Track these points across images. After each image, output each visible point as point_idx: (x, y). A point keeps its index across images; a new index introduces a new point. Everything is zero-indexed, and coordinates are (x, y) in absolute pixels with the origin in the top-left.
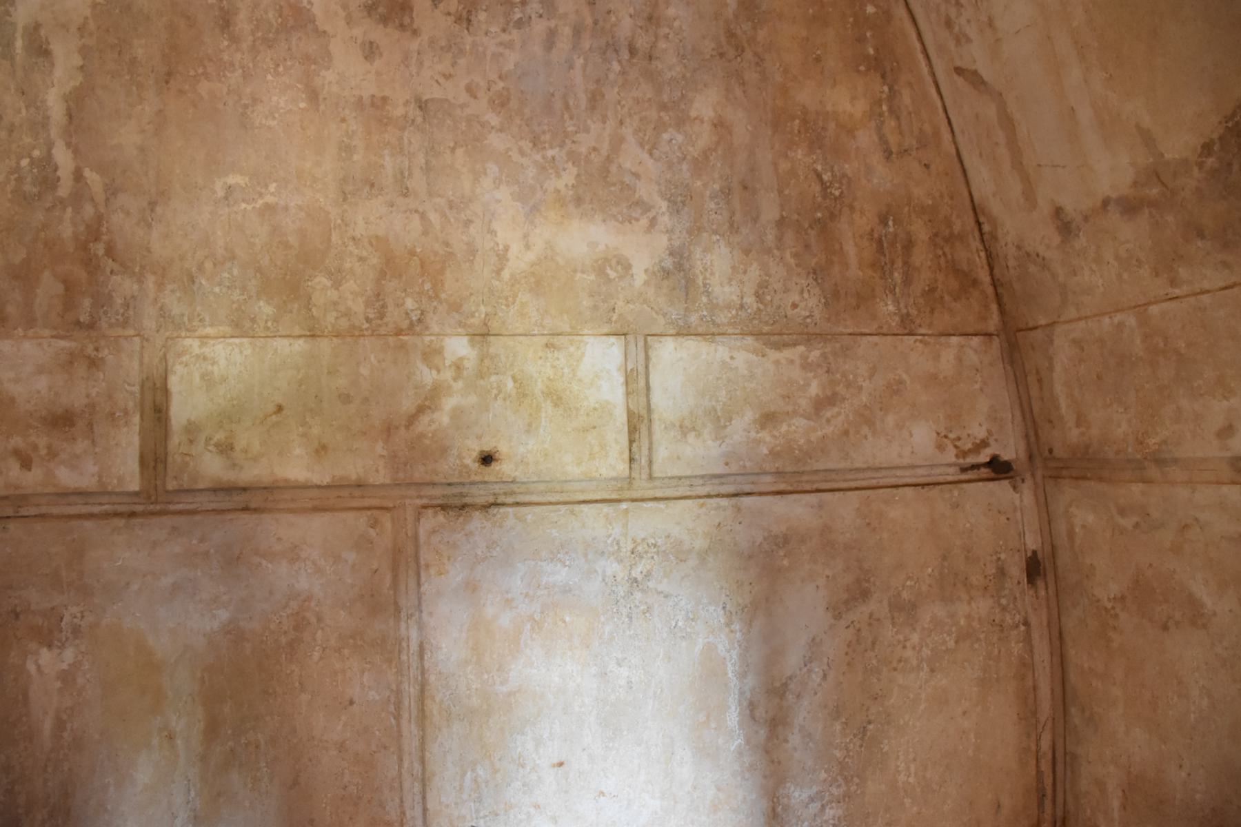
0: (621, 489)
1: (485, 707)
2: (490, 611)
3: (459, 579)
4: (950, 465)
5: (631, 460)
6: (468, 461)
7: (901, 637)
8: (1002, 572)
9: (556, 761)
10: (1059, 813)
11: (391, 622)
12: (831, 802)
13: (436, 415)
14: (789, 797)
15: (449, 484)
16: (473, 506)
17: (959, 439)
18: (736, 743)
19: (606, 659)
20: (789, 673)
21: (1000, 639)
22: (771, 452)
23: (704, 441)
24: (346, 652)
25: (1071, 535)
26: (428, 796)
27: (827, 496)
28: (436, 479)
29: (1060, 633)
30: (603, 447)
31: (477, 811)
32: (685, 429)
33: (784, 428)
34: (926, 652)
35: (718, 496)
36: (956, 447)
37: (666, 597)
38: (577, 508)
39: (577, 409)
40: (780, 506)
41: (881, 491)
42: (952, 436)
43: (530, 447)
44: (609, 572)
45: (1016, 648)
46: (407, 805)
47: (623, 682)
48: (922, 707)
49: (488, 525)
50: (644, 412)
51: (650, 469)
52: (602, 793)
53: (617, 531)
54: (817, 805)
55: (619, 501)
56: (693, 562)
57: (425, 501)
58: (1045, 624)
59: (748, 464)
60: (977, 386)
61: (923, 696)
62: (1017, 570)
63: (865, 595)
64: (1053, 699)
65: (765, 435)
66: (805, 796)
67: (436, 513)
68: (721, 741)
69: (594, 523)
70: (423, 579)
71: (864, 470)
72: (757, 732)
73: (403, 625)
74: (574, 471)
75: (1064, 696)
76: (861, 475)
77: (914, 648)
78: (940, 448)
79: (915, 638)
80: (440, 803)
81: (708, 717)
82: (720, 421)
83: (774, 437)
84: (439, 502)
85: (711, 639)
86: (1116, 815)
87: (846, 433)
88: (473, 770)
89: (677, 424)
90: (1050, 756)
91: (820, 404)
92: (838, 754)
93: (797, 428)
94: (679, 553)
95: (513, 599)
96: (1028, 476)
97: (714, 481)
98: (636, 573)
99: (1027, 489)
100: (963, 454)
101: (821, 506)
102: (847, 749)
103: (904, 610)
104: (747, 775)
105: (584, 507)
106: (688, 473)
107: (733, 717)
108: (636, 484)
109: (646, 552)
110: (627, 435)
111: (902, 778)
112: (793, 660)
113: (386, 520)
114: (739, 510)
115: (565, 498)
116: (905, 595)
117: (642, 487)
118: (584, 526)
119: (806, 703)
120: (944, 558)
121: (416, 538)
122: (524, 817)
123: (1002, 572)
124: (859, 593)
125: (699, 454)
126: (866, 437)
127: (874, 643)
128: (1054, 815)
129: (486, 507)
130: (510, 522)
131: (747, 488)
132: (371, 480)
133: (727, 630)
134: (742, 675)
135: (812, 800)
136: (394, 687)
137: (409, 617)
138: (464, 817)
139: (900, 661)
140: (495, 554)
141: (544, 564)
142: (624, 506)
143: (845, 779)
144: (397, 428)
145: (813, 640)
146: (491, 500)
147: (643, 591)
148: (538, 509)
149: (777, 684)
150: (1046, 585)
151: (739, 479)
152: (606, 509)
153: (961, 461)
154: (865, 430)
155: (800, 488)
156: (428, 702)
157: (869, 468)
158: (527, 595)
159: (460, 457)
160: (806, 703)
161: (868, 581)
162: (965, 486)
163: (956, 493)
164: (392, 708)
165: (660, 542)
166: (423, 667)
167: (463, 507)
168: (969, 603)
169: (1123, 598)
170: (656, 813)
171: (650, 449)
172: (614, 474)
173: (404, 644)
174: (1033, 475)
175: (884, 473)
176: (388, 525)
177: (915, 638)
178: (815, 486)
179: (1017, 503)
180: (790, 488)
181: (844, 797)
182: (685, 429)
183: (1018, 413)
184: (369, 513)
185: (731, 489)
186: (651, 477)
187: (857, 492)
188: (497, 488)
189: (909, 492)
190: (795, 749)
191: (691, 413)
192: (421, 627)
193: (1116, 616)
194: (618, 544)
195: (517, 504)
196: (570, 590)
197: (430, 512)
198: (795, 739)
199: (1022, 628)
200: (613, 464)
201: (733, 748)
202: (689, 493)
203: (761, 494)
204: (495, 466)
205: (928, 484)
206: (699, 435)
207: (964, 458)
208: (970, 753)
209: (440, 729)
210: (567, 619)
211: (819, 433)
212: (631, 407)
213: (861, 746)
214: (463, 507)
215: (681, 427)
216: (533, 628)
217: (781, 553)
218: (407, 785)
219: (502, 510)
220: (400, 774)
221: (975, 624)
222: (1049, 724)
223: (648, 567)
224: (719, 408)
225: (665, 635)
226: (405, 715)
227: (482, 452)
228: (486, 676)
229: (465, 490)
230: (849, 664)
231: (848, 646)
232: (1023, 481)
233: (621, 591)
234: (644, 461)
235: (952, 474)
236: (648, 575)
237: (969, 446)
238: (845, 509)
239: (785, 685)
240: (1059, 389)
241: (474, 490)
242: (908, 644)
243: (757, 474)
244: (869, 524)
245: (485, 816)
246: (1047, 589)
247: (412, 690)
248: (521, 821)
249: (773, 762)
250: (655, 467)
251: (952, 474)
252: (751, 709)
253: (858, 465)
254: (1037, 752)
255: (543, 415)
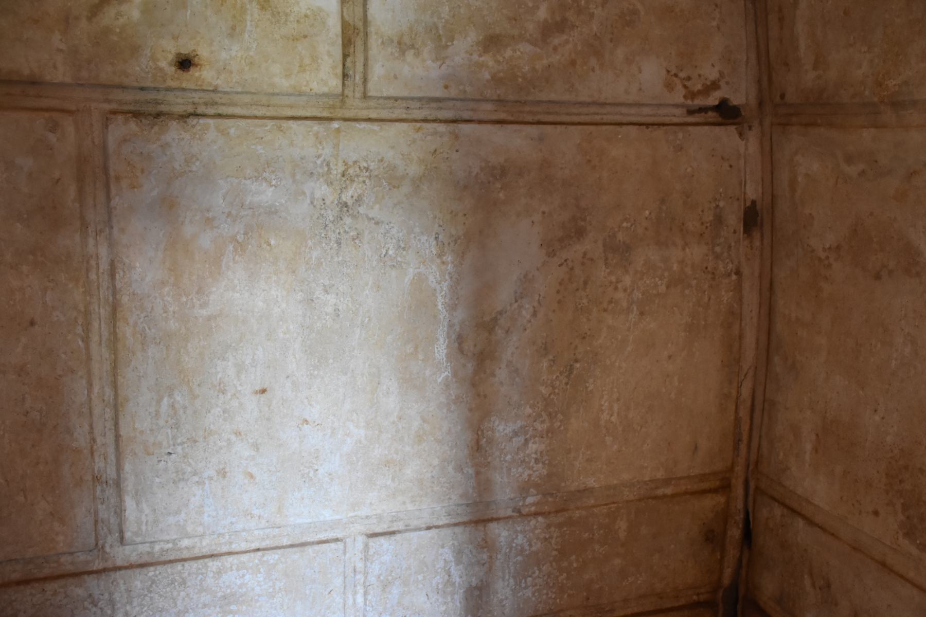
0: (333, 107)
1: (183, 331)
2: (188, 230)
3: (154, 193)
4: (677, 106)
5: (345, 76)
6: (163, 64)
7: (613, 279)
8: (719, 220)
9: (258, 388)
10: (753, 457)
11: (77, 237)
12: (535, 437)
13: (124, 8)
14: (493, 430)
15: (142, 89)
16: (170, 115)
17: (689, 78)
18: (443, 375)
19: (313, 285)
20: (499, 309)
21: (711, 286)
22: (493, 77)
23: (424, 61)
24: (25, 268)
25: (793, 184)
26: (121, 423)
27: (549, 129)
28: (126, 81)
29: (771, 284)
30: (314, 59)
31: (174, 438)
32: (403, 45)
33: (508, 53)
34: (637, 295)
35: (434, 121)
36: (685, 87)
37: (377, 223)
38: (285, 124)
39: (287, 15)
40: (499, 136)
41: (605, 128)
42: (682, 75)
43: (233, 53)
44: (318, 194)
45: (726, 296)
46: (98, 431)
47: (330, 309)
48: (629, 349)
49: (187, 136)
50: (360, 24)
51: (365, 87)
52: (306, 421)
53: (327, 151)
54: (521, 439)
55: (330, 119)
56: (406, 189)
57: (114, 106)
58: (757, 274)
59: (468, 89)
60: (714, 23)
61: (631, 338)
62: (734, 220)
63: (580, 233)
64: (757, 348)
65: (488, 59)
66: (509, 430)
67: (127, 120)
68: (428, 373)
69: (302, 141)
70: (113, 191)
71: (588, 104)
72: (464, 366)
73: (91, 242)
74: (284, 84)
75: (769, 344)
76: (585, 110)
77: (625, 290)
78: (669, 86)
79: (627, 280)
80: (135, 429)
81: (416, 348)
82: (441, 39)
83: (498, 62)
84: (131, 108)
85: (422, 269)
86: (807, 457)
87: (573, 63)
88: (170, 396)
89: (396, 40)
90: (749, 403)
91: (548, 30)
92: (544, 390)
93: (522, 55)
94: (391, 178)
95: (214, 218)
96: (756, 123)
97: (434, 105)
98: (346, 197)
99: (753, 137)
100: (692, 95)
101: (541, 139)
102: (553, 387)
103: (619, 251)
104: (453, 407)
105: (293, 124)
106: (405, 94)
107: (441, 349)
108: (349, 102)
109: (358, 176)
110: (340, 47)
111: (605, 417)
112: (504, 295)
113: (68, 125)
114: (457, 137)
115: (271, 112)
116: (620, 236)
117: (355, 106)
118: (292, 144)
119: (515, 339)
120: (663, 201)
121: (104, 147)
122: (225, 444)
123: (719, 220)
124: (575, 231)
125: (419, 73)
126: (593, 70)
127: (585, 283)
128: (747, 459)
129: (184, 117)
130: (212, 135)
131: (466, 115)
132: (48, 78)
133: (438, 261)
134: (452, 308)
135: (516, 434)
136: (81, 307)
137: (98, 233)
138: (160, 444)
139: (610, 302)
140: (194, 169)
141: (248, 182)
142: (336, 125)
143: (550, 415)
144: (77, 18)
145: (526, 276)
146: (190, 109)
147: (354, 217)
148: (242, 123)
149: (487, 318)
150: (762, 236)
151: (459, 104)
152: (316, 127)
153: (689, 102)
154: (593, 62)
155: (521, 119)
156: (120, 324)
157: (594, 103)
158: (229, 214)
159: (153, 58)
160: (515, 339)
161: (584, 220)
162: (690, 128)
163: (680, 135)
164: (79, 330)
165: (372, 166)
166: (114, 287)
167: (158, 115)
168: (684, 249)
169: (838, 248)
170: (360, 442)
171: (365, 65)
172: (325, 90)
173: (93, 262)
174: (761, 124)
175: (608, 109)
176: (70, 130)
177: (627, 280)
178: (537, 118)
179: (742, 150)
180: (510, 118)
181: (548, 432)
182: (403, 45)
183: (753, 56)
184: (47, 115)
185: (449, 115)
186: (365, 96)
187: (580, 127)
188: (197, 97)
189: (633, 130)
190: (501, 383)
191: (411, 29)
192: (112, 245)
193: (830, 266)
194: (328, 165)
195: (220, 116)
196: (276, 212)
197: (120, 118)
198: (502, 374)
199: (734, 277)
200: (324, 78)
201: (439, 380)
202: (404, 116)
203: (480, 122)
204: (194, 72)
205: (653, 124)
206: (418, 54)
207: (693, 99)
208: (673, 396)
209: (134, 354)
210: (273, 242)
211: (545, 62)
212: (347, 18)
213: (567, 384)
214: (158, 115)
215: (399, 43)
216: (235, 250)
217: (498, 185)
218: (97, 411)
219: (202, 121)
220: (90, 400)
221: (688, 270)
222: (751, 373)
223: (360, 192)
224: (440, 25)
225: (375, 263)
226: (95, 338)
227: (179, 55)
228: (184, 299)
229: (160, 97)
230: (559, 302)
231: (560, 284)
232: (750, 128)
233: (330, 215)
234: (358, 78)
235: (678, 115)
236: (359, 200)
237: (699, 87)
238: (567, 144)
239: (495, 320)
240: (801, 28)
241: (170, 97)
242: (620, 286)
243: (479, 100)
244: (589, 161)
245: (182, 443)
246: (762, 240)
247: (102, 311)
248: (221, 448)
249: (479, 395)
250: (370, 85)
251: (678, 115)
252: (459, 342)
253: (584, 98)
254: (737, 398)
255: (248, 18)
